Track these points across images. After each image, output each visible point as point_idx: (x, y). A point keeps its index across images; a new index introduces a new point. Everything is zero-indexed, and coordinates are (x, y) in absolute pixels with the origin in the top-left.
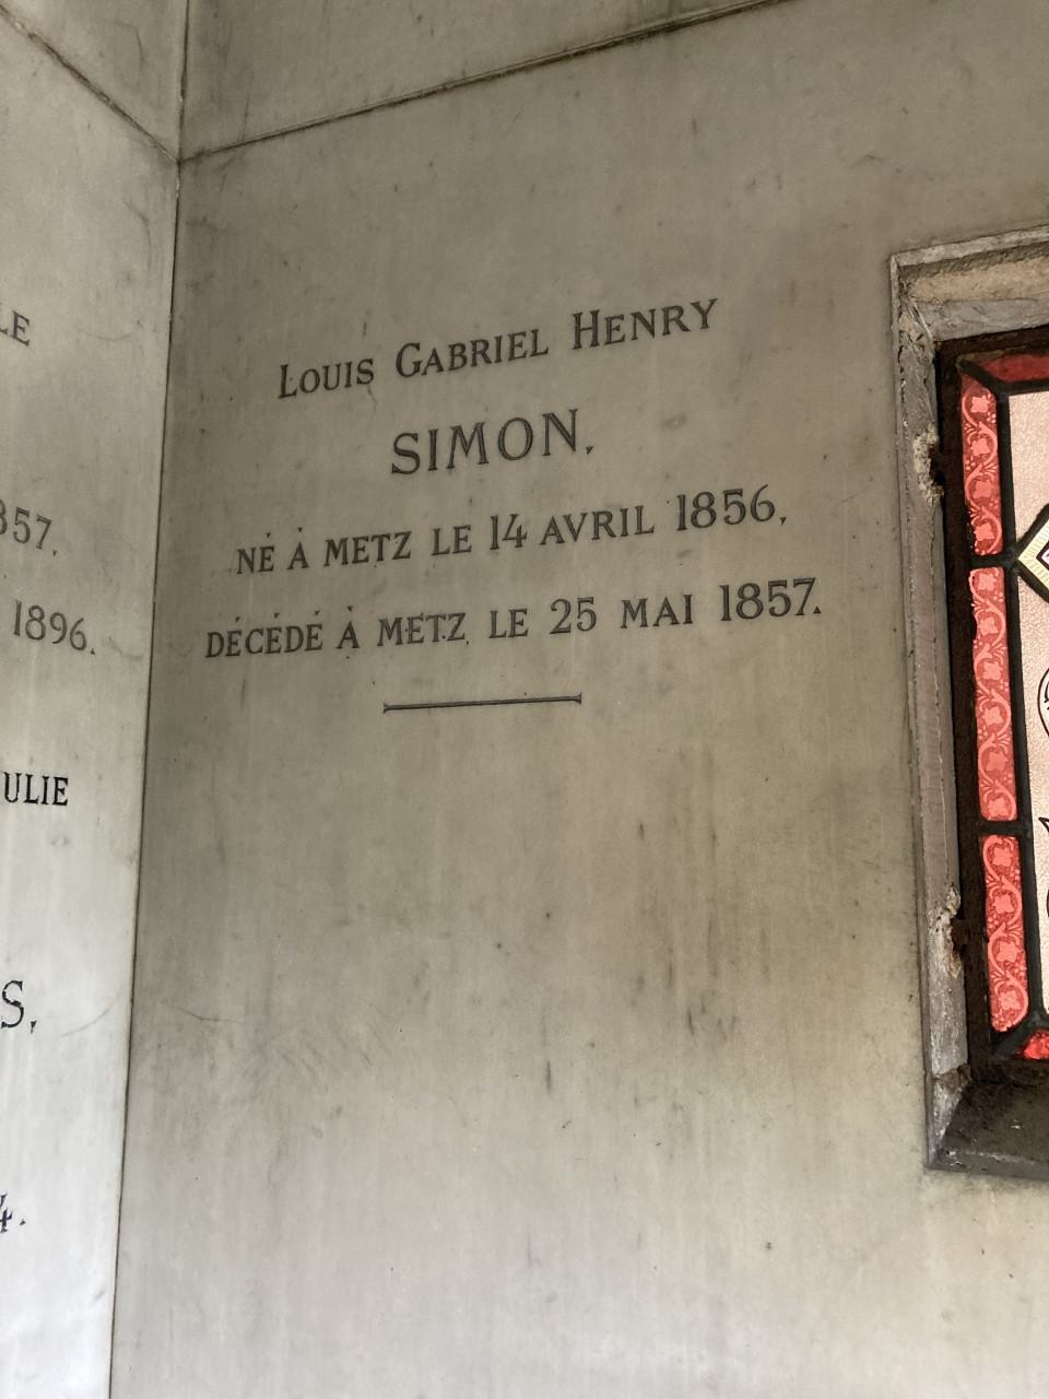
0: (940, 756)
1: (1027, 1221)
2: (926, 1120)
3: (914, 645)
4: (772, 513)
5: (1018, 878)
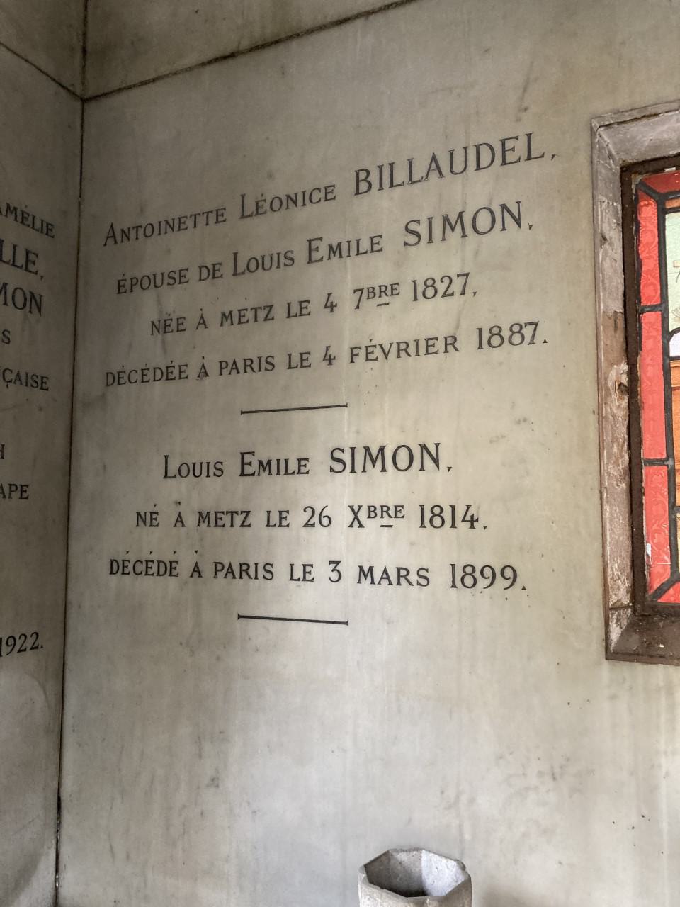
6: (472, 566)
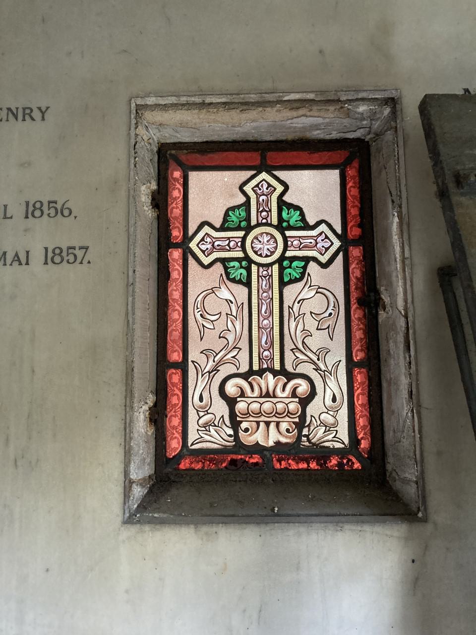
0: (148, 333)
1: (164, 543)
2: (124, 501)
3: (134, 279)
4: (70, 214)
5: (181, 388)
6: (58, 248)
